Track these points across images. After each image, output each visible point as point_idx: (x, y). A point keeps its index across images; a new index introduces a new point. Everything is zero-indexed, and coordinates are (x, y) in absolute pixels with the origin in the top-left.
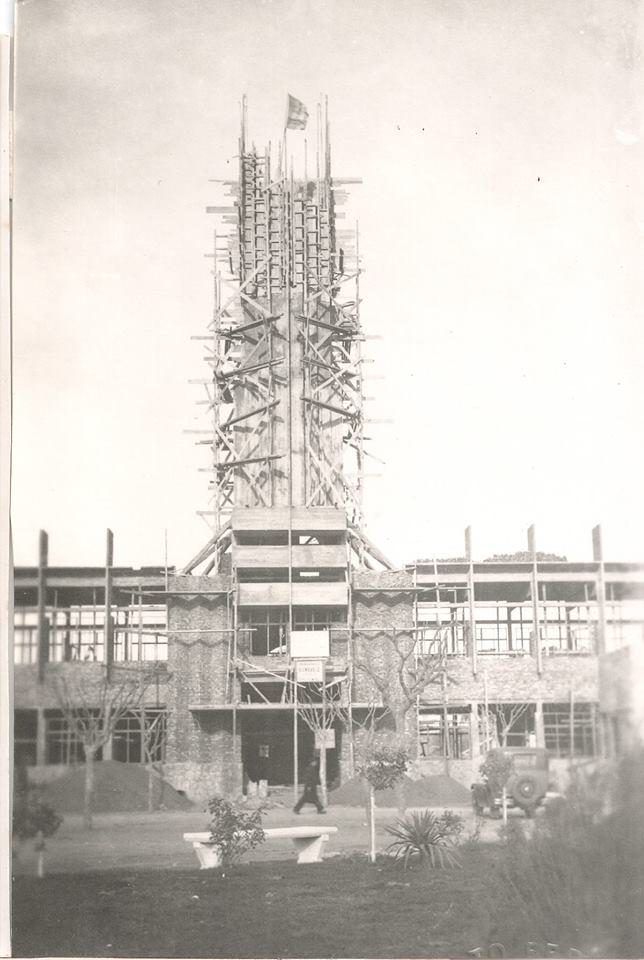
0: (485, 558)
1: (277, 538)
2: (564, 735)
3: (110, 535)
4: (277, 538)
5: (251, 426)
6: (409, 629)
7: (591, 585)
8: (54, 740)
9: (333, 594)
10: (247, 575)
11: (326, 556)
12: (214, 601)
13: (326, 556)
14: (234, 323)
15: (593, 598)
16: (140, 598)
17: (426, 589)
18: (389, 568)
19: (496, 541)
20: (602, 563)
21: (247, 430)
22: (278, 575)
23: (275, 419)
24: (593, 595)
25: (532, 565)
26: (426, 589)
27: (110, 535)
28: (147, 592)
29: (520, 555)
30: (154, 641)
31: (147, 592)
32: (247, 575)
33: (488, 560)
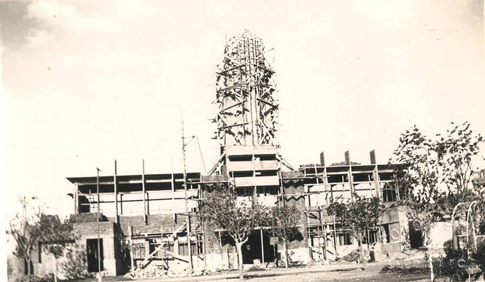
0: (331, 164)
1: (247, 158)
2: (273, 222)
3: (143, 161)
4: (247, 158)
5: (232, 112)
6: (303, 195)
7: (346, 176)
8: (75, 239)
9: (273, 181)
10: (238, 174)
11: (268, 165)
12: (297, 183)
13: (268, 165)
14: (29, 220)
15: (372, 180)
16: (191, 186)
17: (311, 178)
18: (292, 170)
19: (334, 159)
20: (376, 165)
21: (230, 114)
22: (249, 174)
23: (245, 110)
24: (372, 178)
25: (349, 167)
26: (311, 178)
27: (143, 161)
28: (194, 183)
29: (342, 163)
30: (120, 203)
31: (194, 183)
32: (238, 174)
33: (333, 165)
